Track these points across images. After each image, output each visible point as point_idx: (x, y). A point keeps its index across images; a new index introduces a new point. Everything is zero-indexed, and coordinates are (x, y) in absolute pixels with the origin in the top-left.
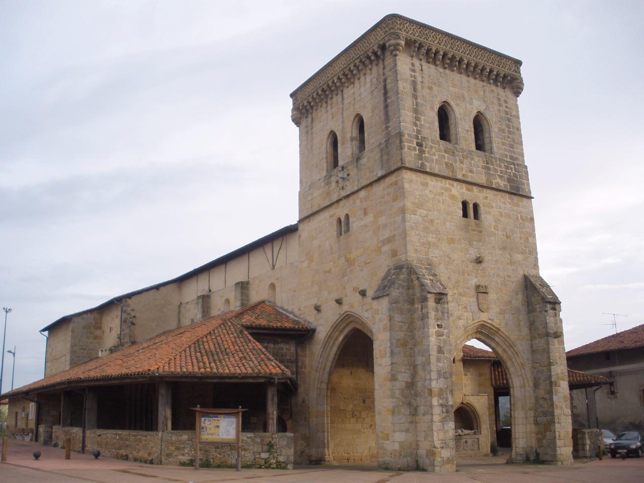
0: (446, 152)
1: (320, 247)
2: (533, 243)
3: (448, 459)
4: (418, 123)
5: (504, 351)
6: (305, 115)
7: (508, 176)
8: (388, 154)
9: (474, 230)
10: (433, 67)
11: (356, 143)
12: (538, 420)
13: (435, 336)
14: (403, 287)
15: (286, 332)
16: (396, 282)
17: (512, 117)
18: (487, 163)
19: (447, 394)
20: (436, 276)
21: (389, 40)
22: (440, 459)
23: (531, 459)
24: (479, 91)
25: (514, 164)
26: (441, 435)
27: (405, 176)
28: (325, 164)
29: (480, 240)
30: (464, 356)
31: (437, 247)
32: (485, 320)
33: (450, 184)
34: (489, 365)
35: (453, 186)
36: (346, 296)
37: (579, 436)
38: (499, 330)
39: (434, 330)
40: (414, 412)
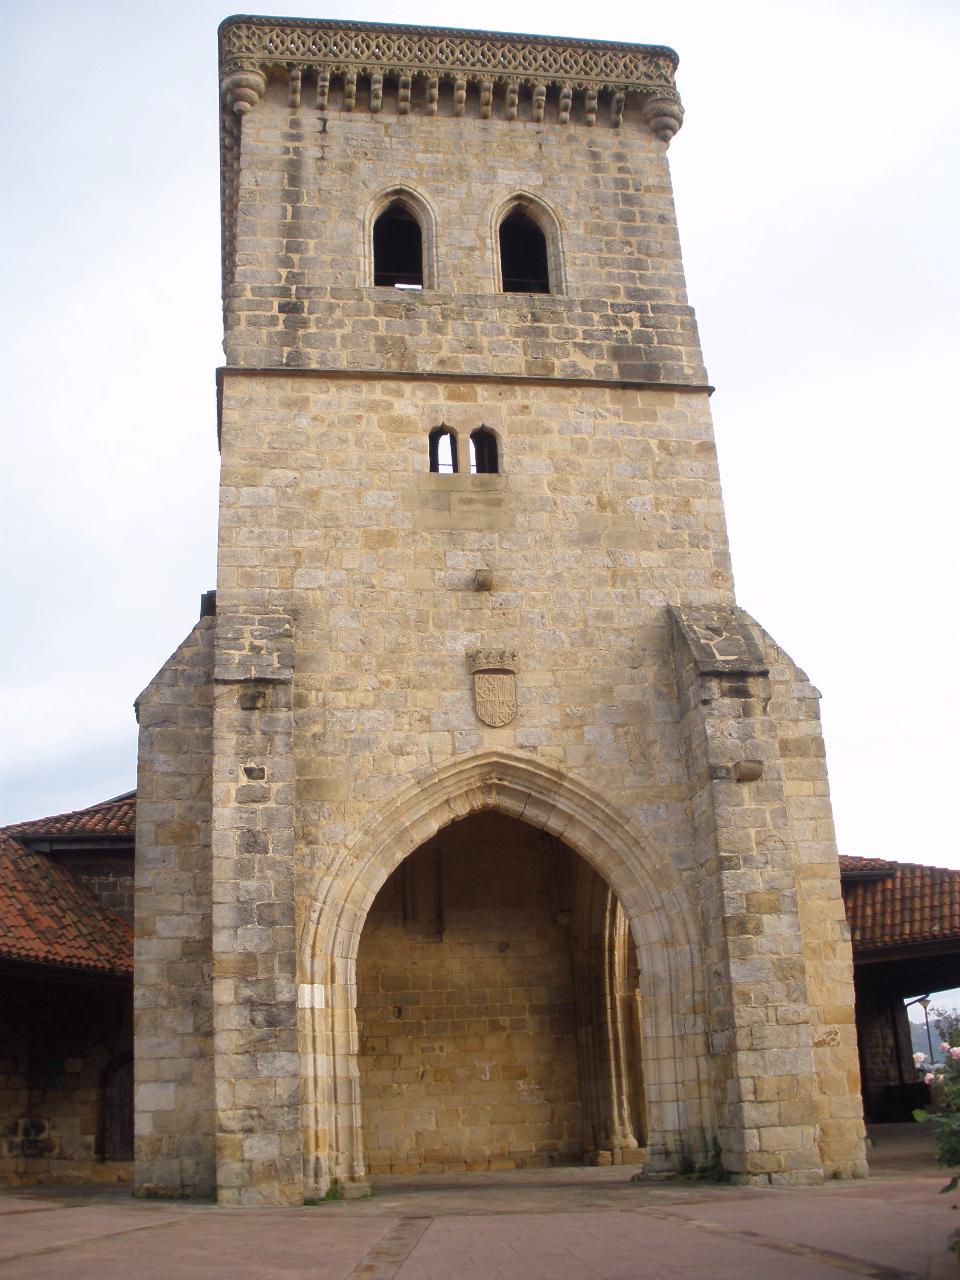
4: (295, 257)
7: (613, 343)
13: (234, 804)
14: (189, 679)
19: (270, 970)
22: (237, 1166)
25: (641, 309)
26: (245, 1092)
32: (500, 749)
35: (399, 394)
38: (562, 776)
39: (233, 788)
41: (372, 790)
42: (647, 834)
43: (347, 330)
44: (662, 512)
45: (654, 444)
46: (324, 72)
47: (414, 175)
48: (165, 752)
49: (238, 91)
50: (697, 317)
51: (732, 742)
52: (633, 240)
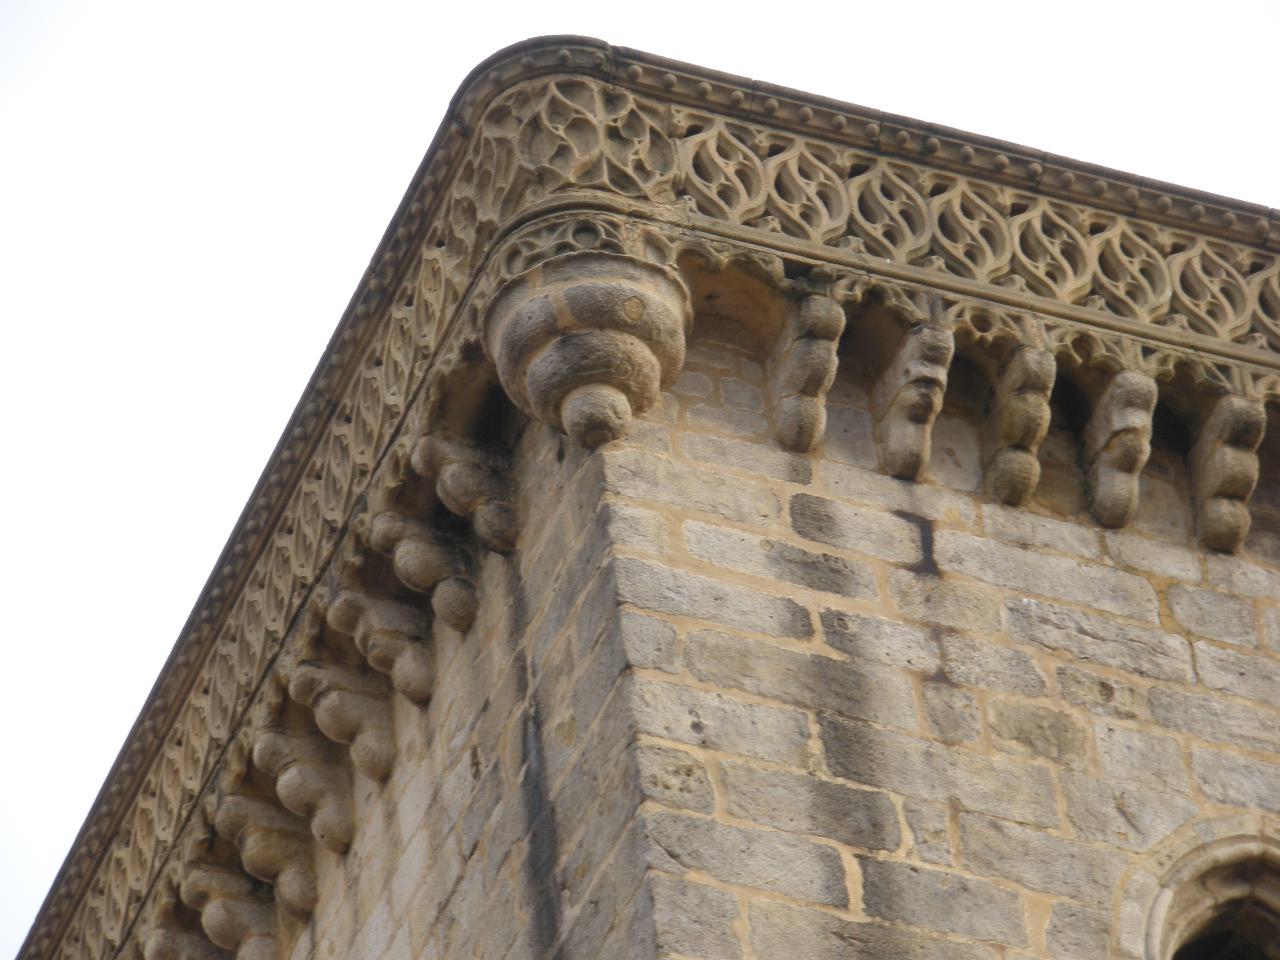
21: (507, 289)
46: (933, 323)
49: (599, 339)
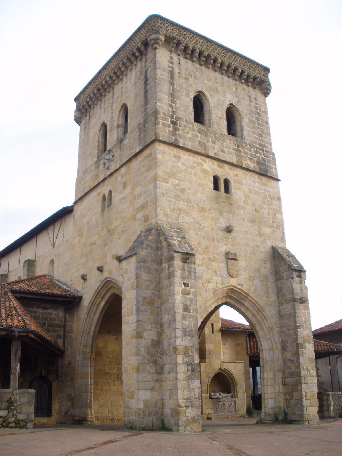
0: (199, 132)
1: (88, 222)
2: (280, 219)
3: (193, 418)
4: (174, 105)
5: (254, 315)
6: (85, 114)
8: (145, 131)
9: (224, 202)
10: (190, 62)
11: (121, 130)
12: (286, 381)
13: (180, 295)
14: (151, 248)
15: (53, 298)
16: (144, 242)
17: (261, 112)
18: (238, 146)
19: (192, 352)
20: (185, 238)
21: (150, 35)
22: (184, 419)
23: (280, 419)
24: (231, 87)
25: (263, 150)
26: (186, 394)
27: (158, 148)
28: (97, 152)
29: (230, 212)
30: (222, 327)
31: (188, 214)
32: (234, 285)
33: (202, 160)
34: (245, 336)
35: (205, 161)
36: (106, 264)
37: (325, 398)
38: (248, 295)
39: (180, 289)
40: (160, 371)
41: (202, 293)
42: (269, 315)
43: (190, 135)
44: (270, 216)
45: (267, 194)
46: (183, 44)
47: (204, 87)
48: (145, 272)
50: (276, 156)
51: (299, 291)
52: (260, 127)
